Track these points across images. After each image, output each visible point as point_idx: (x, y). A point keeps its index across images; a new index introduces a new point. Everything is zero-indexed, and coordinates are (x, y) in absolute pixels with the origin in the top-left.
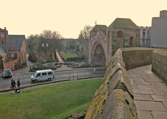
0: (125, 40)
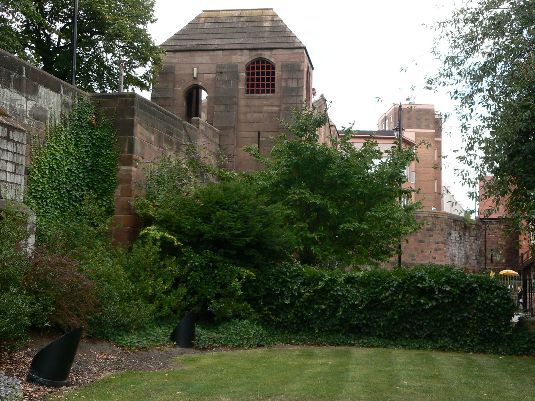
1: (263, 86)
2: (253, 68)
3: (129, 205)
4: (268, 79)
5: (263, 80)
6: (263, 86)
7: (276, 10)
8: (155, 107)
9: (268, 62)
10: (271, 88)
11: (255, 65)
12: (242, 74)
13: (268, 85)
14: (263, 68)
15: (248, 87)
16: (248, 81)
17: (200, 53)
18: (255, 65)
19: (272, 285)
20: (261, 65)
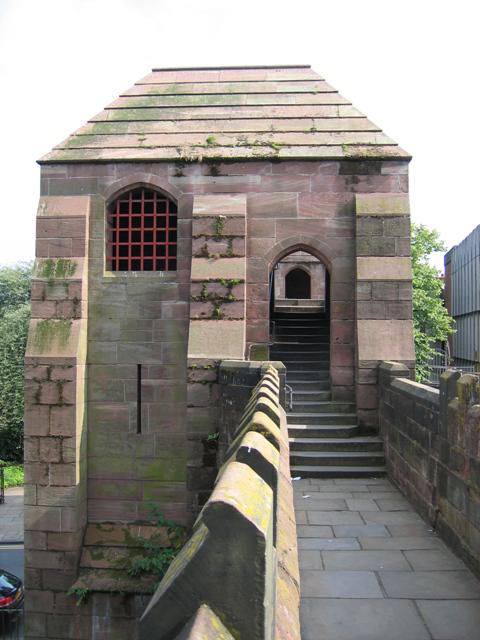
0: (195, 290)
1: (148, 251)
2: (124, 208)
3: (189, 467)
4: (161, 236)
5: (149, 236)
6: (148, 251)
7: (379, 96)
8: (321, 214)
9: (161, 195)
10: (167, 258)
11: (131, 201)
12: (149, 178)
13: (161, 251)
14: (149, 208)
15: (114, 255)
16: (114, 241)
17: (290, 163)
18: (131, 201)
19: (434, 504)
20: (143, 201)
